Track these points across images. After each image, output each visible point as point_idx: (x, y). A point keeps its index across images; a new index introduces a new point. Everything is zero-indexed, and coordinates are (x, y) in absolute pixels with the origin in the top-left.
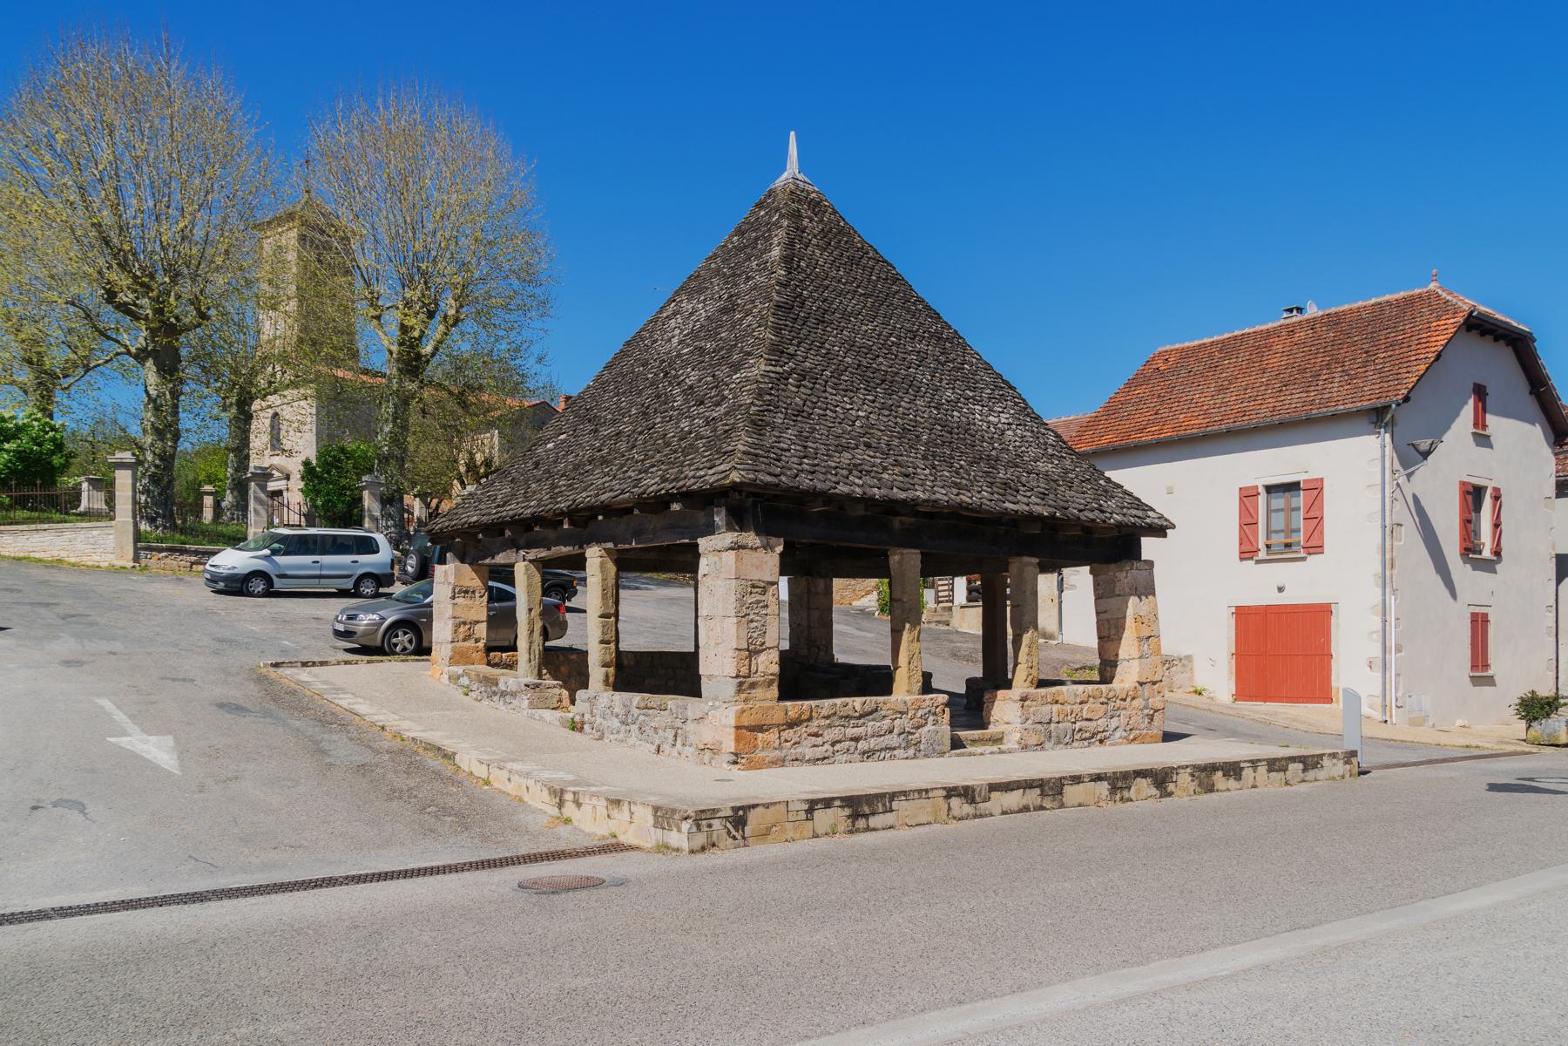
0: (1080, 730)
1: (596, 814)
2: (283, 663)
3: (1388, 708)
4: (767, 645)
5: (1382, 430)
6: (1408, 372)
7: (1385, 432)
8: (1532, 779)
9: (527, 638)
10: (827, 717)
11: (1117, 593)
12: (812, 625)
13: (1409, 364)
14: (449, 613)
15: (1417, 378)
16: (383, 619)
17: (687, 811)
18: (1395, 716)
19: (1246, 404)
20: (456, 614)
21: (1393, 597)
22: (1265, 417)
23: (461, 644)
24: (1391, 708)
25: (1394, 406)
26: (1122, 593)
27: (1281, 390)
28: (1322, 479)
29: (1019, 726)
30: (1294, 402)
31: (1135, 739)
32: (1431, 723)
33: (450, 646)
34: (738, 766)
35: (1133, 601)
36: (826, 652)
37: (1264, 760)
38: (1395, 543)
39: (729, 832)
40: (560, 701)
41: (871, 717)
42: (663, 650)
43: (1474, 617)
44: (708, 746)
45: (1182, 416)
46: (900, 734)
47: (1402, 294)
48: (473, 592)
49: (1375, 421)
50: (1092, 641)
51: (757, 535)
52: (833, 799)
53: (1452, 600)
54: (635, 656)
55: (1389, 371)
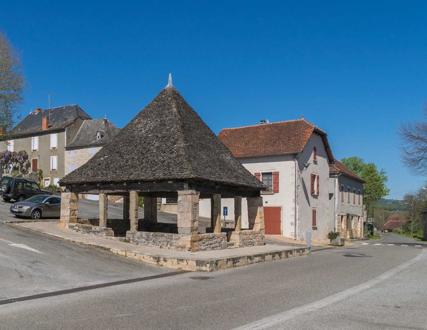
1: (173, 263)
2: (13, 222)
5: (296, 160)
6: (301, 144)
7: (296, 160)
8: (349, 254)
10: (206, 239)
11: (255, 205)
13: (301, 142)
14: (69, 207)
16: (32, 208)
17: (208, 261)
18: (298, 238)
19: (256, 149)
21: (298, 205)
22: (263, 153)
23: (72, 217)
25: (299, 153)
27: (265, 146)
28: (278, 172)
29: (239, 241)
30: (270, 150)
32: (305, 240)
33: (69, 217)
34: (190, 251)
36: (155, 219)
39: (215, 267)
41: (213, 238)
43: (313, 210)
45: (237, 151)
46: (218, 243)
47: (294, 120)
48: (75, 201)
49: (294, 157)
50: (209, 216)
52: (230, 259)
53: (309, 206)
54: (112, 220)
55: (296, 143)
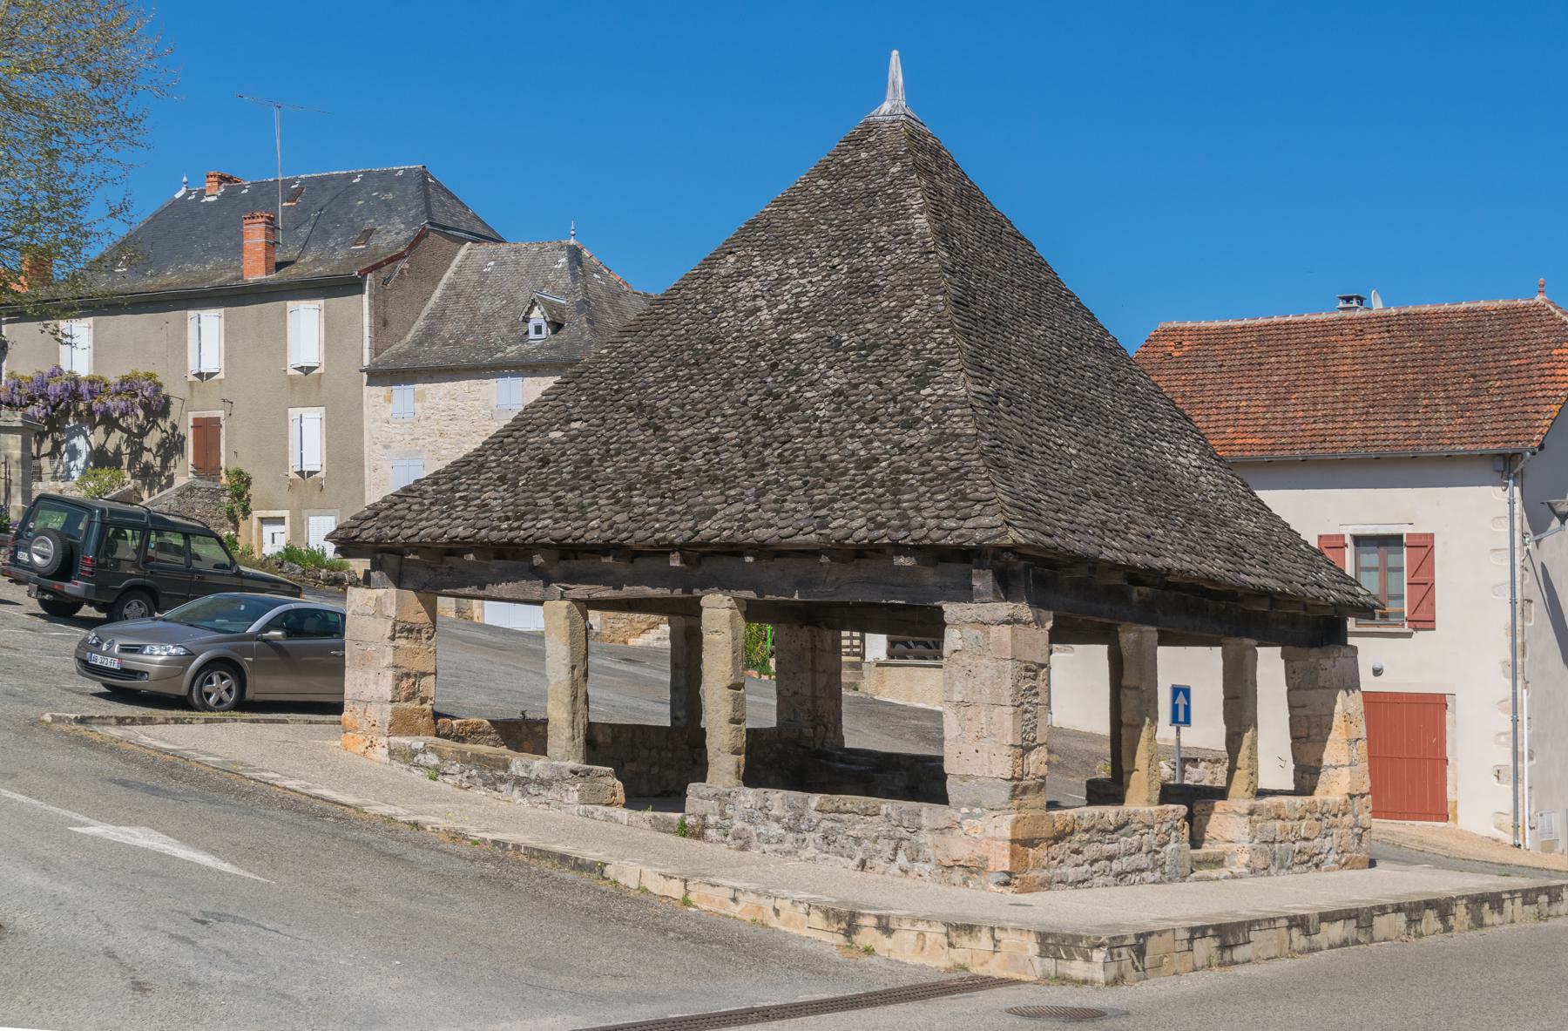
0: (1300, 852)
2: (92, 717)
3: (1520, 830)
4: (1038, 741)
5: (1511, 482)
6: (1538, 412)
7: (1515, 485)
9: (569, 707)
10: (1087, 831)
11: (1321, 684)
12: (818, 694)
15: (1551, 421)
16: (191, 655)
20: (399, 662)
24: (1524, 830)
26: (1327, 684)
27: (1367, 413)
29: (1247, 845)
30: (1391, 431)
31: (1345, 864)
33: (389, 707)
35: (1341, 695)
36: (835, 732)
37: (1520, 891)
38: (1526, 624)
39: (1133, 963)
40: (614, 794)
41: (1122, 831)
42: (647, 723)
44: (961, 863)
46: (1147, 853)
48: (419, 631)
50: (1101, 725)
51: (1030, 607)
52: (1207, 927)
55: (1512, 407)
